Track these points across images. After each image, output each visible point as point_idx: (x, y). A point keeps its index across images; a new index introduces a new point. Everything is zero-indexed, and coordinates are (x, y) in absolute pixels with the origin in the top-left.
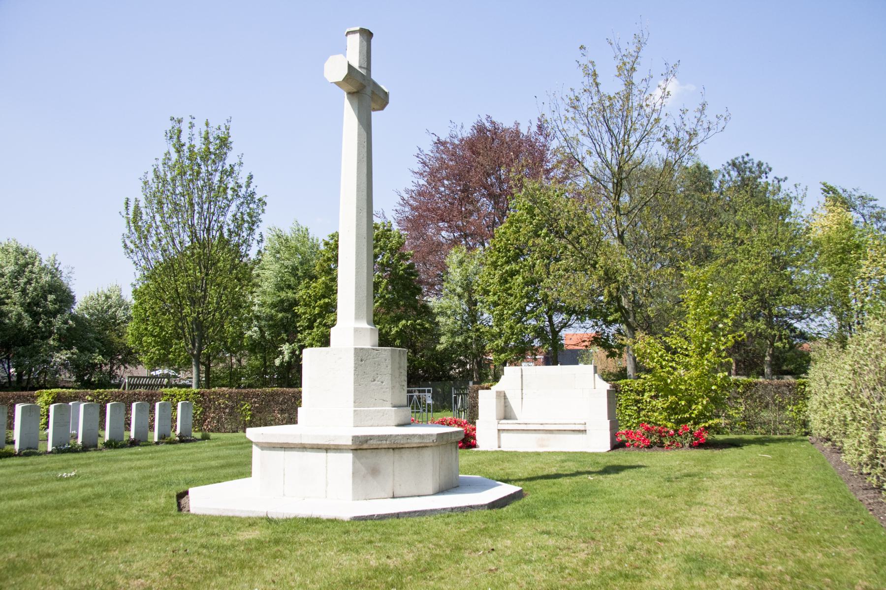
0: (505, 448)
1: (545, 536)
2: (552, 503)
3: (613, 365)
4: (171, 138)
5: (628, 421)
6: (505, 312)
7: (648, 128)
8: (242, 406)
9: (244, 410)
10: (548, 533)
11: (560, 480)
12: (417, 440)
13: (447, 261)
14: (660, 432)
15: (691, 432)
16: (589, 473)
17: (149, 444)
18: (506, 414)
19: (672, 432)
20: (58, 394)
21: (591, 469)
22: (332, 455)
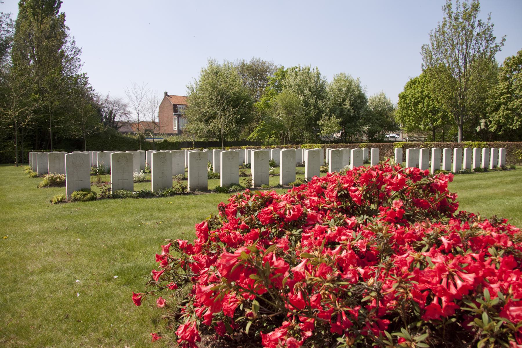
4: (445, 9)
9: (517, 153)
20: (405, 144)
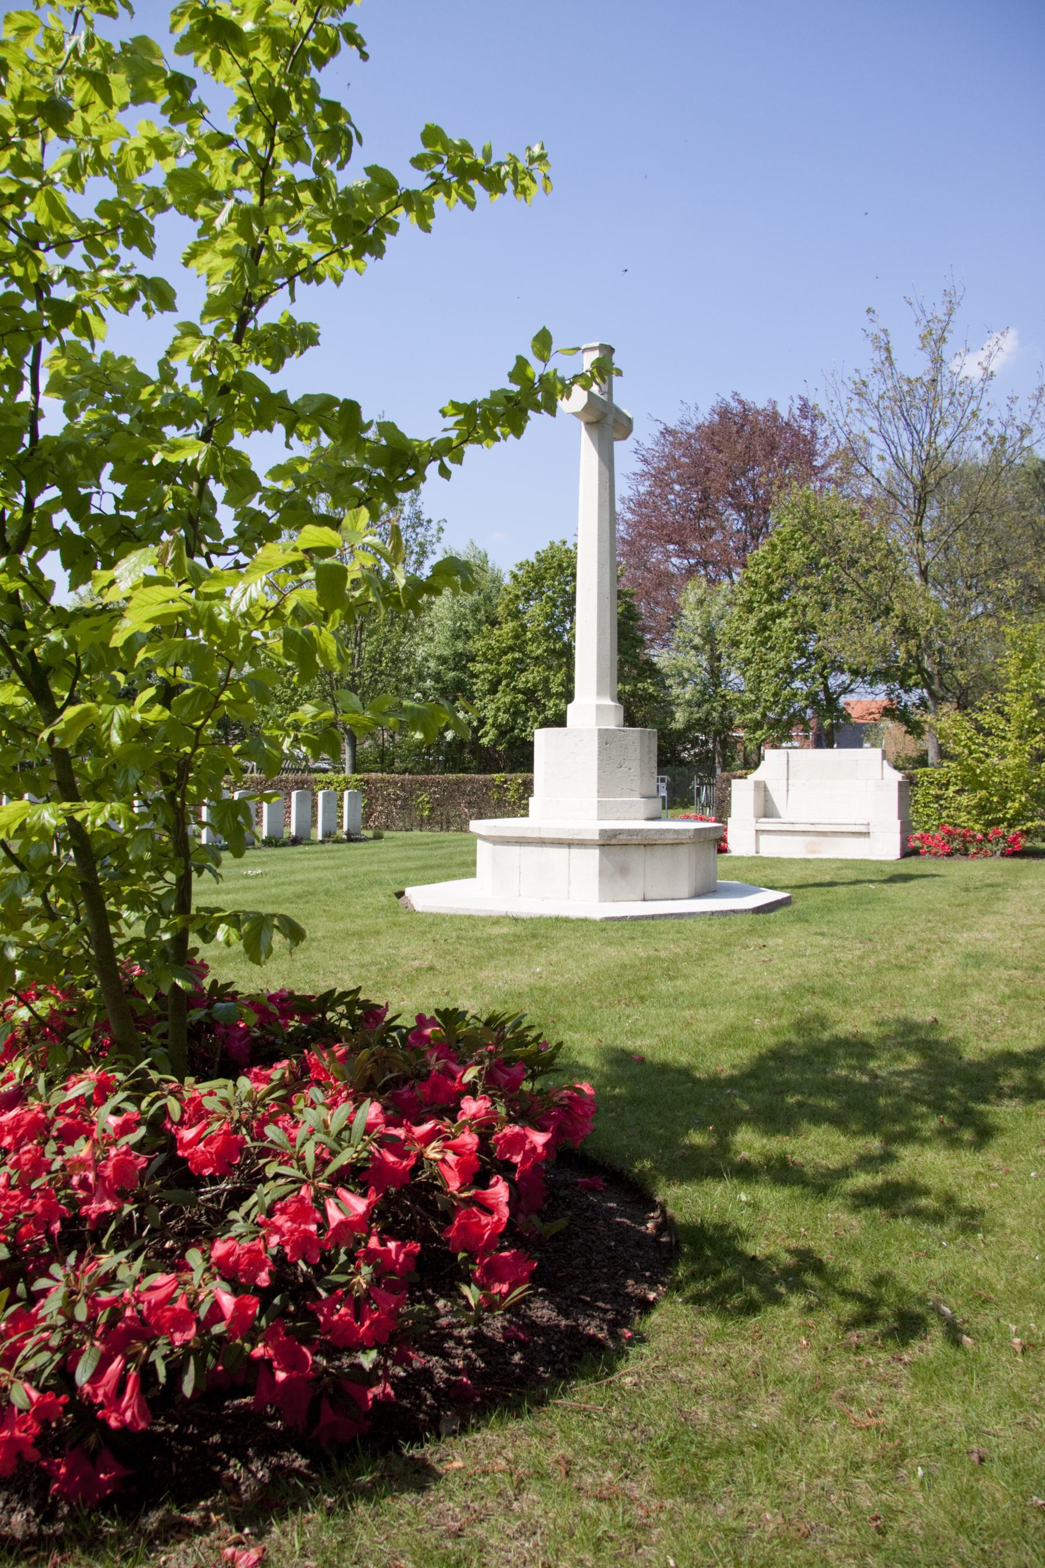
0: (765, 852)
1: (820, 938)
2: (826, 909)
3: (910, 746)
5: (926, 823)
6: (764, 672)
7: (964, 422)
8: (418, 797)
10: (823, 934)
11: (836, 888)
12: (671, 836)
13: (680, 601)
14: (964, 836)
15: (1004, 837)
16: (871, 881)
17: (312, 843)
18: (767, 809)
19: (979, 836)
21: (873, 878)
22: (575, 852)
